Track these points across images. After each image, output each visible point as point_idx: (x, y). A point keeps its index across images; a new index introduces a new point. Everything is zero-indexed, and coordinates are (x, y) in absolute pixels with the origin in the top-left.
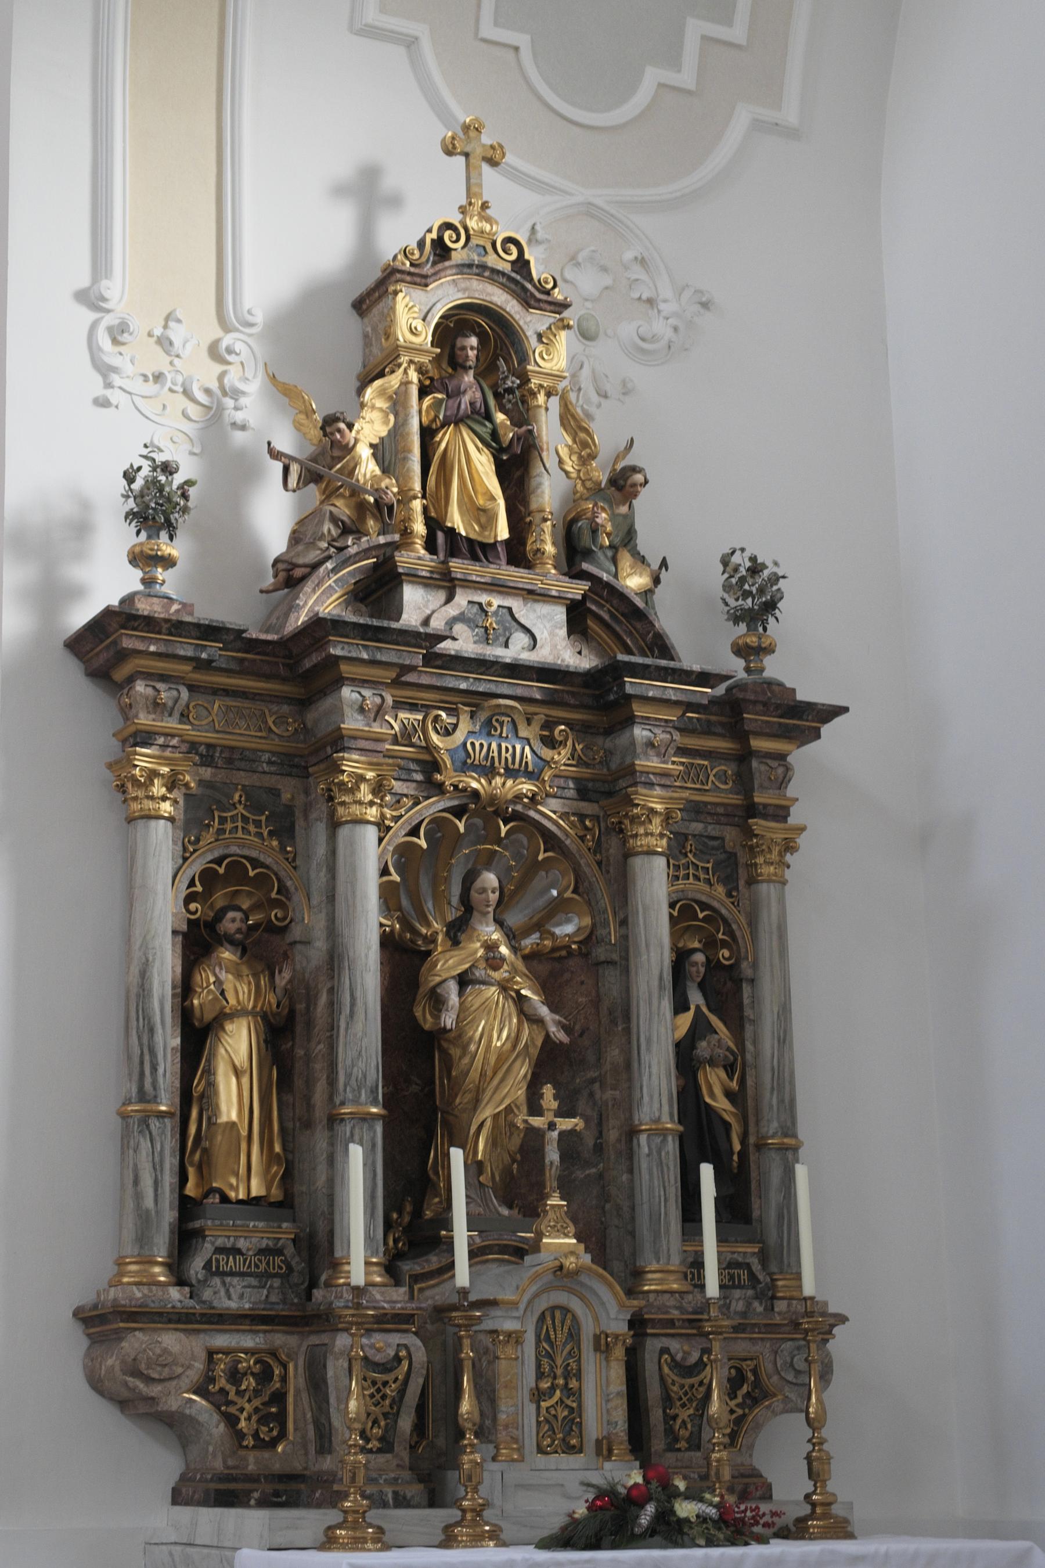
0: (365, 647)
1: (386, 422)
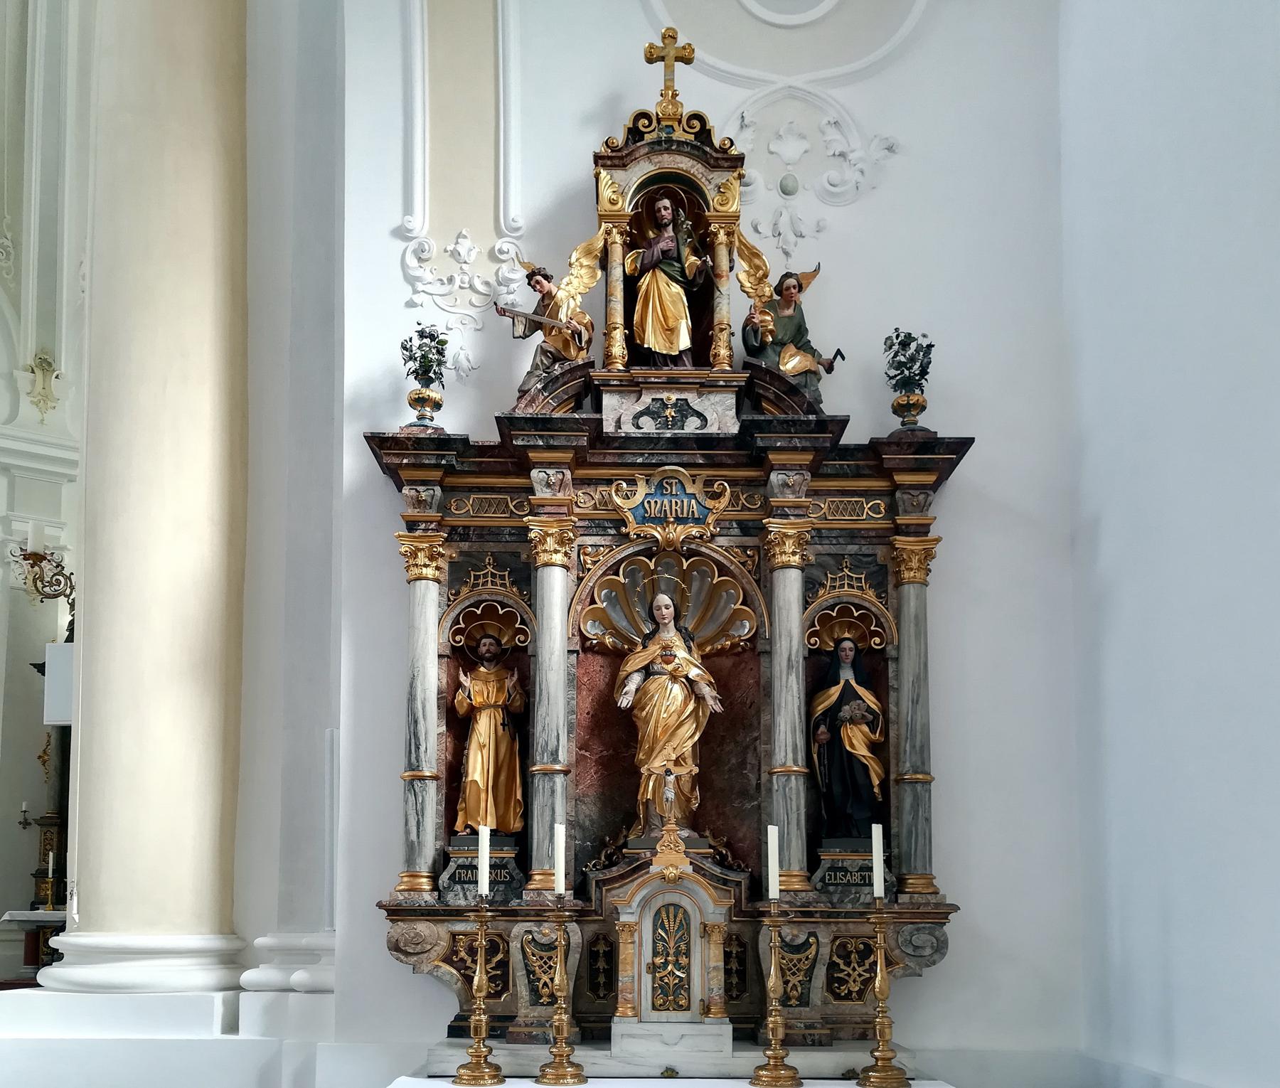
0: (541, 437)
1: (593, 276)
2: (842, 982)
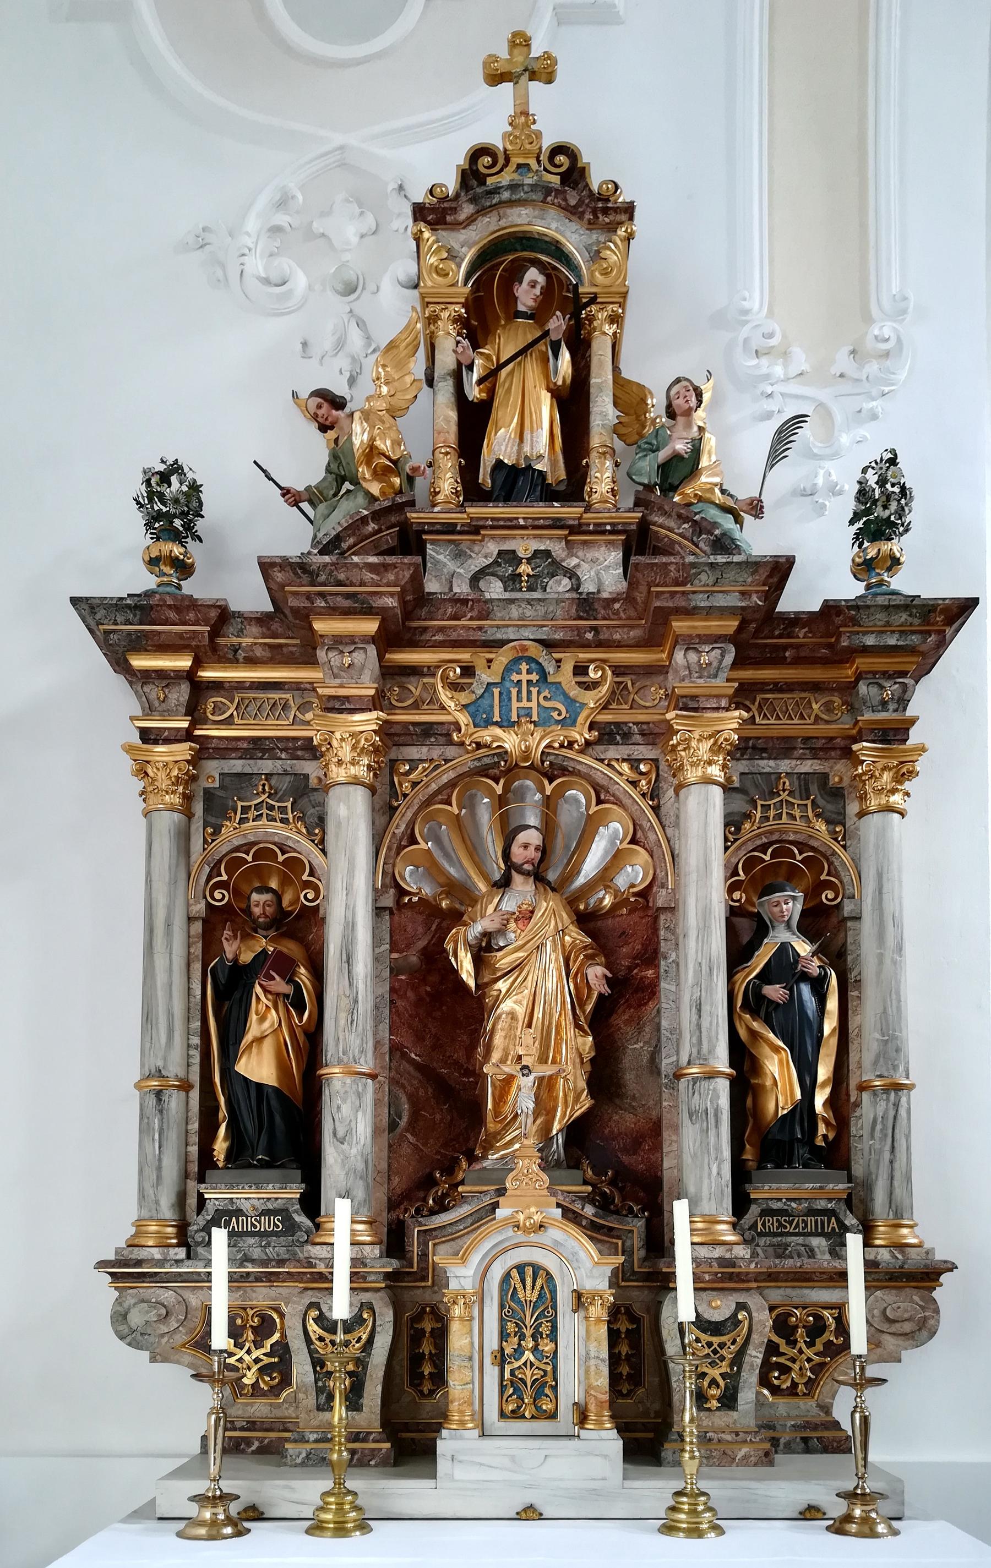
2: (785, 1370)
